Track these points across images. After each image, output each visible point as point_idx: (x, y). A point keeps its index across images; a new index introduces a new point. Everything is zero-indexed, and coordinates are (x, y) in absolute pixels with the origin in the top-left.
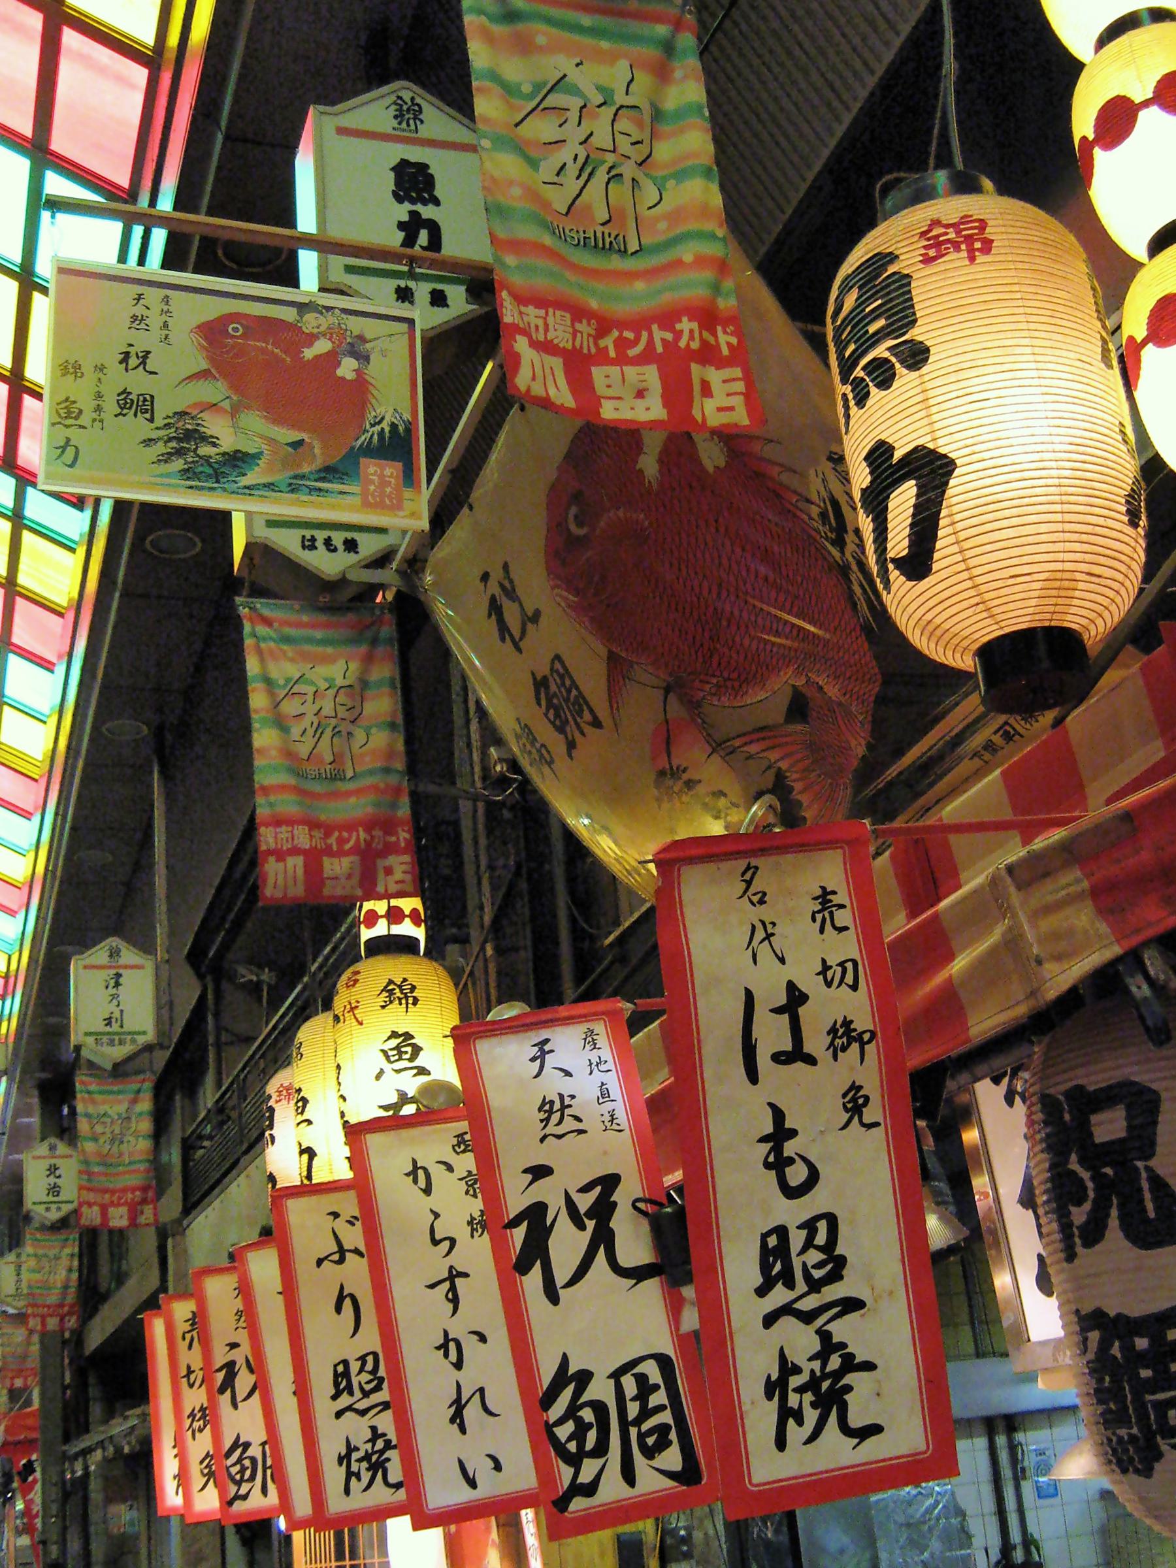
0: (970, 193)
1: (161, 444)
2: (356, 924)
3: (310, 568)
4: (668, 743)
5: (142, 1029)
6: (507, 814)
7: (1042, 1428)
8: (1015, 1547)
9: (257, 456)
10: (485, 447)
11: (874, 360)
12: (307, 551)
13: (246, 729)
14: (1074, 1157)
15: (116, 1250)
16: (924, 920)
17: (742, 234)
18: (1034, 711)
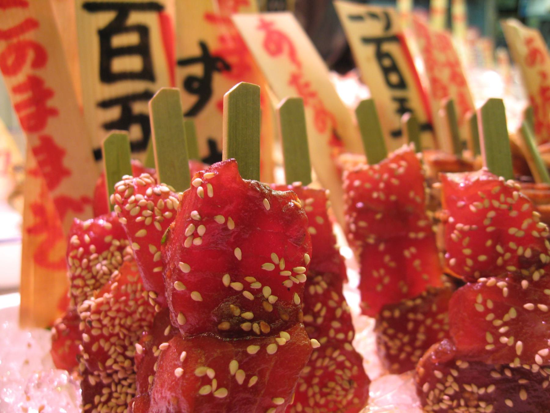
6: (303, 362)
7: (251, 312)
8: (364, 312)
12: (67, 162)
15: (440, 57)
18: (215, 177)
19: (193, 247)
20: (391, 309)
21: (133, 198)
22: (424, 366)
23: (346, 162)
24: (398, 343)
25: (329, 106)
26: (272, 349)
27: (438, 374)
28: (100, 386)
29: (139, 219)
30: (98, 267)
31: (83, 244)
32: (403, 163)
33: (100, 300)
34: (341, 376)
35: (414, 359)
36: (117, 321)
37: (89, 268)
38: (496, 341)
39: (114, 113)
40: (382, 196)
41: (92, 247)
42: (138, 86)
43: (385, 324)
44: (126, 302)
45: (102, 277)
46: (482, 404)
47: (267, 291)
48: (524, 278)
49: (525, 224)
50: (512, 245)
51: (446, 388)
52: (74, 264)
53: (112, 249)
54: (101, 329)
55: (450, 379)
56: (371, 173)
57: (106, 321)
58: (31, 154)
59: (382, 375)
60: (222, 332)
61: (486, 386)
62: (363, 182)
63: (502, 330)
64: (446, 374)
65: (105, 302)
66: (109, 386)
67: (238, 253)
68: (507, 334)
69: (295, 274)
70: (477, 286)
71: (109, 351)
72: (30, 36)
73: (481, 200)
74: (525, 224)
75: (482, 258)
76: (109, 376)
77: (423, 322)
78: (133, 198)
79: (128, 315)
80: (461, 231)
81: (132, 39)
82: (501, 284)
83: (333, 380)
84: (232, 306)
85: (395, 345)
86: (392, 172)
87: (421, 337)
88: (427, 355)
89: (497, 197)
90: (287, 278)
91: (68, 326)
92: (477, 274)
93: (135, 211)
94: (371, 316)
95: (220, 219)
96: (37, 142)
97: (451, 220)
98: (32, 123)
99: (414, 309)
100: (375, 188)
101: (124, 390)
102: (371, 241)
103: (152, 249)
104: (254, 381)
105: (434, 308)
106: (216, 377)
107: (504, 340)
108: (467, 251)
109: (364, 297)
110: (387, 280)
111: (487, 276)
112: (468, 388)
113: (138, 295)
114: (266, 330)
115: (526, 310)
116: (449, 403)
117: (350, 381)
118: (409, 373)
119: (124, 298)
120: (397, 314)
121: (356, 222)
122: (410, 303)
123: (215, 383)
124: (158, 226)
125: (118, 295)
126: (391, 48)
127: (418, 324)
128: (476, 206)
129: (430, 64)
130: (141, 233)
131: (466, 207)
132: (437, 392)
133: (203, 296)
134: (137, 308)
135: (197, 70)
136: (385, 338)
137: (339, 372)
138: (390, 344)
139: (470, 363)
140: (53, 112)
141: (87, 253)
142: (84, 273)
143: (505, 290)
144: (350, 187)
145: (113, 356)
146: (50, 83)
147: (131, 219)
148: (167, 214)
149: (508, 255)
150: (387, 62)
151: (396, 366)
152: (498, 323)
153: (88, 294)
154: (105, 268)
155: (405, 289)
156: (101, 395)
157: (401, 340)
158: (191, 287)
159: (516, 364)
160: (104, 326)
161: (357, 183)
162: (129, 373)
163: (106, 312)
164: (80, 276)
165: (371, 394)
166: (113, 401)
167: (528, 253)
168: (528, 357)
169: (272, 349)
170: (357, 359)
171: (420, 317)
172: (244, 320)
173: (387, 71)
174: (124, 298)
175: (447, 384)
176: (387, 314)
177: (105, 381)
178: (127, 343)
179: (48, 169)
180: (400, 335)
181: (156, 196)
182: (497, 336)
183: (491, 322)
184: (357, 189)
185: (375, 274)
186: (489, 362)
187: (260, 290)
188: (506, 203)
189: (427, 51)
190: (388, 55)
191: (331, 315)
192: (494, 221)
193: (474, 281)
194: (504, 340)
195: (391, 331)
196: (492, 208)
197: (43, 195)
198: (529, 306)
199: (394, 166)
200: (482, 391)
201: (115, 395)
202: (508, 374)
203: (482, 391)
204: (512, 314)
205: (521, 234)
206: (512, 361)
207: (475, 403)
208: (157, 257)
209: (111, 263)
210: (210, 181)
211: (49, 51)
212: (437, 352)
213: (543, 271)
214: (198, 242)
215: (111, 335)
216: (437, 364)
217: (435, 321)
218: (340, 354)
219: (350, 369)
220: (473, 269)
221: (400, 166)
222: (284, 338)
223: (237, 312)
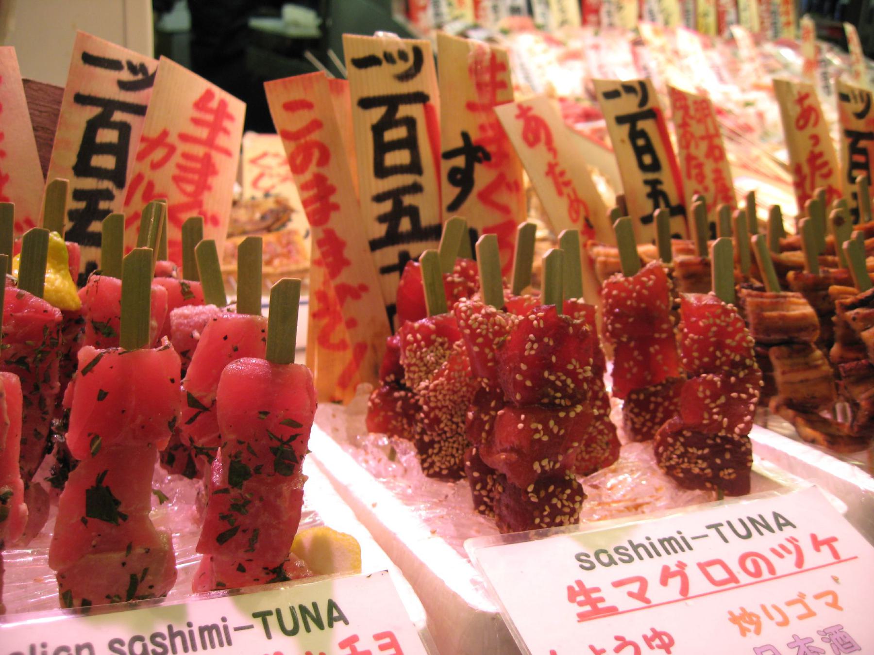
0: (38, 618)
1: (386, 71)
2: (590, 425)
3: (43, 610)
4: (97, 292)
5: (852, 555)
9: (80, 461)
10: (39, 133)
11: (126, 222)
12: (347, 253)
13: (175, 349)
14: (544, 251)
15: (697, 129)
16: (518, 254)
17: (40, 89)
19: (529, 355)
20: (637, 393)
21: (473, 316)
22: (661, 435)
23: (598, 255)
24: (642, 419)
25: (581, 195)
26: (572, 414)
27: (670, 440)
28: (432, 443)
29: (479, 331)
30: (428, 357)
31: (416, 340)
32: (653, 277)
33: (436, 382)
34: (601, 440)
35: (653, 432)
36: (447, 397)
37: (421, 359)
38: (710, 418)
39: (387, 206)
40: (635, 304)
41: (423, 343)
42: (407, 179)
43: (632, 405)
44: (454, 384)
45: (431, 366)
46: (700, 461)
47: (569, 381)
48: (733, 375)
49: (738, 337)
50: (727, 352)
51: (675, 450)
52: (410, 356)
53: (436, 344)
54: (436, 402)
55: (678, 444)
56: (626, 284)
57: (440, 397)
58: (316, 246)
59: (627, 444)
60: (543, 404)
61: (703, 449)
62: (620, 291)
63: (715, 410)
64: (676, 440)
65: (440, 383)
66: (439, 442)
67: (554, 359)
68: (718, 413)
69: (585, 371)
70: (700, 380)
71: (442, 417)
72: (315, 136)
73: (707, 318)
74: (738, 337)
75: (706, 359)
76: (439, 435)
77: (661, 404)
78: (473, 316)
79: (454, 392)
80: (692, 339)
81: (399, 133)
82: (716, 379)
83: (596, 442)
84: (549, 389)
85: (639, 421)
86: (643, 284)
87: (660, 415)
88: (663, 427)
89: (719, 317)
90: (580, 373)
91: (382, 400)
92: (701, 371)
93: (475, 325)
94: (621, 398)
95: (546, 340)
96: (321, 235)
97: (686, 330)
98: (317, 217)
99: (655, 394)
100: (629, 297)
101: (451, 445)
102: (624, 339)
103: (487, 350)
104: (562, 432)
105: (671, 393)
106: (543, 429)
107: (716, 417)
108: (696, 354)
109: (616, 383)
110: (635, 370)
111: (708, 373)
112: (690, 450)
113: (462, 379)
114: (569, 403)
115: (733, 398)
116: (677, 460)
117: (607, 444)
118: (649, 441)
119: (453, 381)
120: (642, 397)
121: (612, 324)
122: (652, 389)
123: (542, 432)
124: (491, 336)
125: (449, 379)
126: (647, 125)
127: (658, 405)
128: (703, 322)
129: (686, 140)
130: (480, 340)
131: (696, 322)
132: (669, 453)
133: (532, 382)
134: (461, 389)
135: (460, 161)
136: (632, 416)
137: (600, 437)
138: (636, 420)
139: (693, 432)
140: (336, 207)
141: (419, 347)
142: (418, 362)
143: (719, 383)
144: (608, 296)
145: (445, 421)
146: (332, 180)
147: (473, 331)
148: (496, 327)
149: (724, 359)
150: (641, 142)
151: (639, 437)
152: (713, 405)
153: (423, 377)
154: (433, 359)
155: (649, 378)
156: (433, 448)
157: (644, 417)
158: (526, 377)
159: (722, 433)
160: (438, 400)
161: (615, 292)
162: (454, 433)
163: (441, 390)
164: (415, 365)
165: (621, 454)
166: (443, 453)
167: (738, 358)
168: (730, 428)
169: (572, 414)
170: (612, 428)
171: (660, 400)
172: (556, 398)
173: (639, 152)
174: (453, 381)
175: (676, 447)
176: (634, 396)
177: (437, 439)
178: (453, 412)
179: (330, 259)
180: (643, 414)
181: (488, 316)
182: (711, 414)
183: (707, 405)
184: (614, 297)
185: (626, 365)
186: (705, 432)
187: (565, 381)
188: (724, 321)
189: (683, 126)
190: (643, 134)
191: (595, 397)
192: (716, 334)
193: (699, 376)
194: (716, 417)
195: (636, 410)
196: (715, 324)
197: (325, 283)
198: (734, 395)
199: (645, 279)
200: (700, 452)
201: (444, 448)
202: (718, 441)
203: (700, 452)
204: (722, 400)
205: (734, 344)
206: (720, 431)
207: (694, 460)
208: (490, 356)
209: (436, 355)
210: (541, 318)
211: (332, 149)
212: (670, 425)
213: (746, 371)
214: (533, 352)
215: (443, 407)
216: (670, 433)
217: (671, 403)
218: (601, 424)
219: (607, 435)
220: (699, 367)
221: (650, 279)
222: (579, 408)
223: (552, 393)
